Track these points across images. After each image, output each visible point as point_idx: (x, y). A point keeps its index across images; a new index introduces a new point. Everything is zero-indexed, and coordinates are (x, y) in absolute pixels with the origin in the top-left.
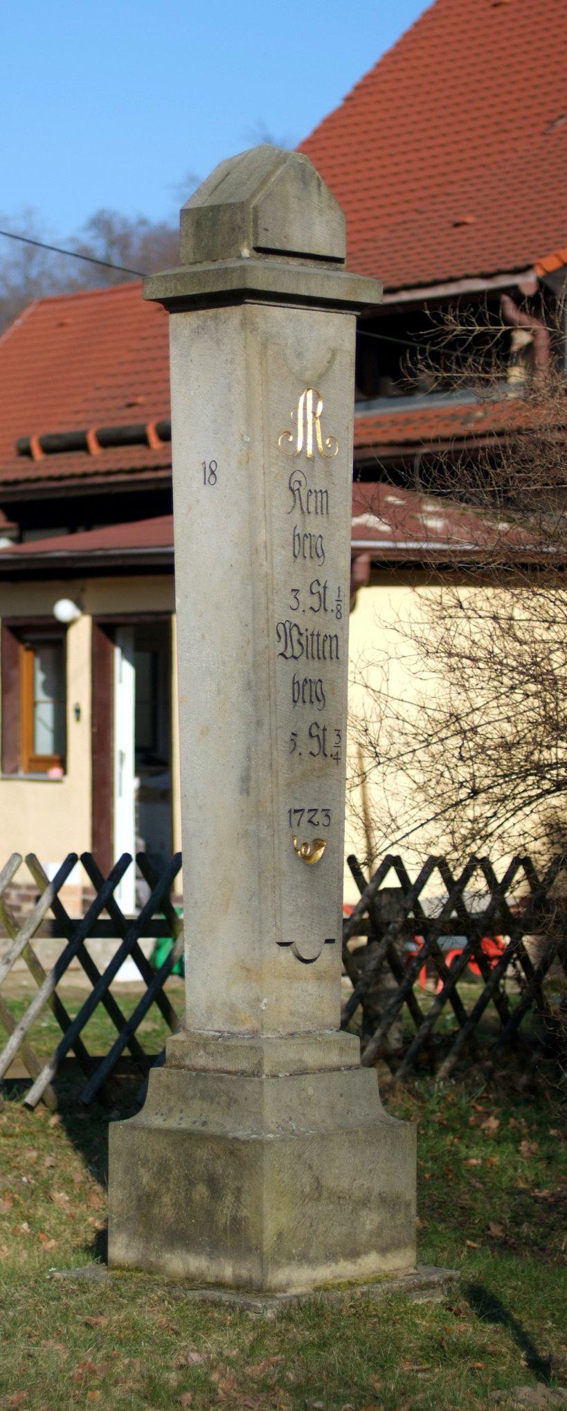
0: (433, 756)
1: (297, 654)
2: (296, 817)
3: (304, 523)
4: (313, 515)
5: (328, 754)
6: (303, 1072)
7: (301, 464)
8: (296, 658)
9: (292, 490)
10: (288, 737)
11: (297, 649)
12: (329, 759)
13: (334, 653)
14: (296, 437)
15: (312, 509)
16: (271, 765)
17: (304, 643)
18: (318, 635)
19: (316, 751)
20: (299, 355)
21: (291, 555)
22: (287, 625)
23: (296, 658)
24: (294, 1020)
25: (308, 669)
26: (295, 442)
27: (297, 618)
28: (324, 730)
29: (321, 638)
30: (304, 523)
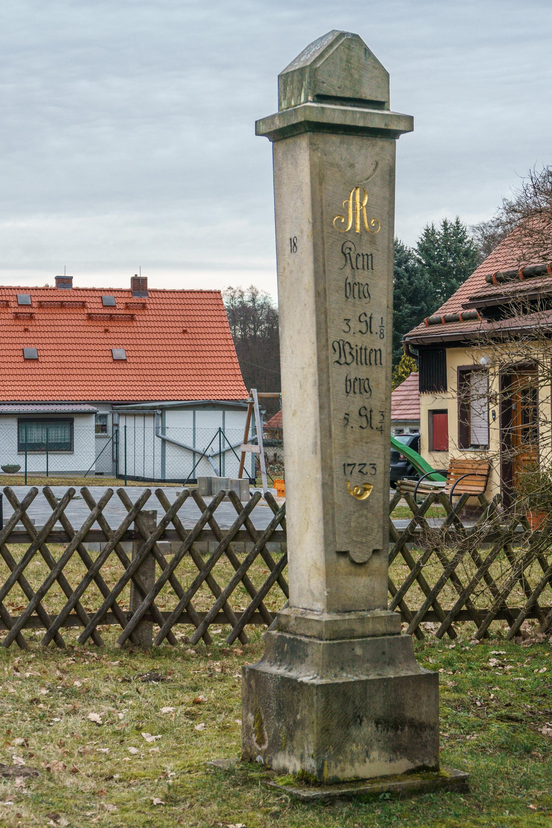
7: (350, 237)
10: (342, 416)
11: (349, 359)
13: (370, 265)
15: (360, 266)
17: (354, 354)
18: (366, 349)
19: (364, 425)
22: (341, 343)
27: (348, 338)
29: (368, 352)
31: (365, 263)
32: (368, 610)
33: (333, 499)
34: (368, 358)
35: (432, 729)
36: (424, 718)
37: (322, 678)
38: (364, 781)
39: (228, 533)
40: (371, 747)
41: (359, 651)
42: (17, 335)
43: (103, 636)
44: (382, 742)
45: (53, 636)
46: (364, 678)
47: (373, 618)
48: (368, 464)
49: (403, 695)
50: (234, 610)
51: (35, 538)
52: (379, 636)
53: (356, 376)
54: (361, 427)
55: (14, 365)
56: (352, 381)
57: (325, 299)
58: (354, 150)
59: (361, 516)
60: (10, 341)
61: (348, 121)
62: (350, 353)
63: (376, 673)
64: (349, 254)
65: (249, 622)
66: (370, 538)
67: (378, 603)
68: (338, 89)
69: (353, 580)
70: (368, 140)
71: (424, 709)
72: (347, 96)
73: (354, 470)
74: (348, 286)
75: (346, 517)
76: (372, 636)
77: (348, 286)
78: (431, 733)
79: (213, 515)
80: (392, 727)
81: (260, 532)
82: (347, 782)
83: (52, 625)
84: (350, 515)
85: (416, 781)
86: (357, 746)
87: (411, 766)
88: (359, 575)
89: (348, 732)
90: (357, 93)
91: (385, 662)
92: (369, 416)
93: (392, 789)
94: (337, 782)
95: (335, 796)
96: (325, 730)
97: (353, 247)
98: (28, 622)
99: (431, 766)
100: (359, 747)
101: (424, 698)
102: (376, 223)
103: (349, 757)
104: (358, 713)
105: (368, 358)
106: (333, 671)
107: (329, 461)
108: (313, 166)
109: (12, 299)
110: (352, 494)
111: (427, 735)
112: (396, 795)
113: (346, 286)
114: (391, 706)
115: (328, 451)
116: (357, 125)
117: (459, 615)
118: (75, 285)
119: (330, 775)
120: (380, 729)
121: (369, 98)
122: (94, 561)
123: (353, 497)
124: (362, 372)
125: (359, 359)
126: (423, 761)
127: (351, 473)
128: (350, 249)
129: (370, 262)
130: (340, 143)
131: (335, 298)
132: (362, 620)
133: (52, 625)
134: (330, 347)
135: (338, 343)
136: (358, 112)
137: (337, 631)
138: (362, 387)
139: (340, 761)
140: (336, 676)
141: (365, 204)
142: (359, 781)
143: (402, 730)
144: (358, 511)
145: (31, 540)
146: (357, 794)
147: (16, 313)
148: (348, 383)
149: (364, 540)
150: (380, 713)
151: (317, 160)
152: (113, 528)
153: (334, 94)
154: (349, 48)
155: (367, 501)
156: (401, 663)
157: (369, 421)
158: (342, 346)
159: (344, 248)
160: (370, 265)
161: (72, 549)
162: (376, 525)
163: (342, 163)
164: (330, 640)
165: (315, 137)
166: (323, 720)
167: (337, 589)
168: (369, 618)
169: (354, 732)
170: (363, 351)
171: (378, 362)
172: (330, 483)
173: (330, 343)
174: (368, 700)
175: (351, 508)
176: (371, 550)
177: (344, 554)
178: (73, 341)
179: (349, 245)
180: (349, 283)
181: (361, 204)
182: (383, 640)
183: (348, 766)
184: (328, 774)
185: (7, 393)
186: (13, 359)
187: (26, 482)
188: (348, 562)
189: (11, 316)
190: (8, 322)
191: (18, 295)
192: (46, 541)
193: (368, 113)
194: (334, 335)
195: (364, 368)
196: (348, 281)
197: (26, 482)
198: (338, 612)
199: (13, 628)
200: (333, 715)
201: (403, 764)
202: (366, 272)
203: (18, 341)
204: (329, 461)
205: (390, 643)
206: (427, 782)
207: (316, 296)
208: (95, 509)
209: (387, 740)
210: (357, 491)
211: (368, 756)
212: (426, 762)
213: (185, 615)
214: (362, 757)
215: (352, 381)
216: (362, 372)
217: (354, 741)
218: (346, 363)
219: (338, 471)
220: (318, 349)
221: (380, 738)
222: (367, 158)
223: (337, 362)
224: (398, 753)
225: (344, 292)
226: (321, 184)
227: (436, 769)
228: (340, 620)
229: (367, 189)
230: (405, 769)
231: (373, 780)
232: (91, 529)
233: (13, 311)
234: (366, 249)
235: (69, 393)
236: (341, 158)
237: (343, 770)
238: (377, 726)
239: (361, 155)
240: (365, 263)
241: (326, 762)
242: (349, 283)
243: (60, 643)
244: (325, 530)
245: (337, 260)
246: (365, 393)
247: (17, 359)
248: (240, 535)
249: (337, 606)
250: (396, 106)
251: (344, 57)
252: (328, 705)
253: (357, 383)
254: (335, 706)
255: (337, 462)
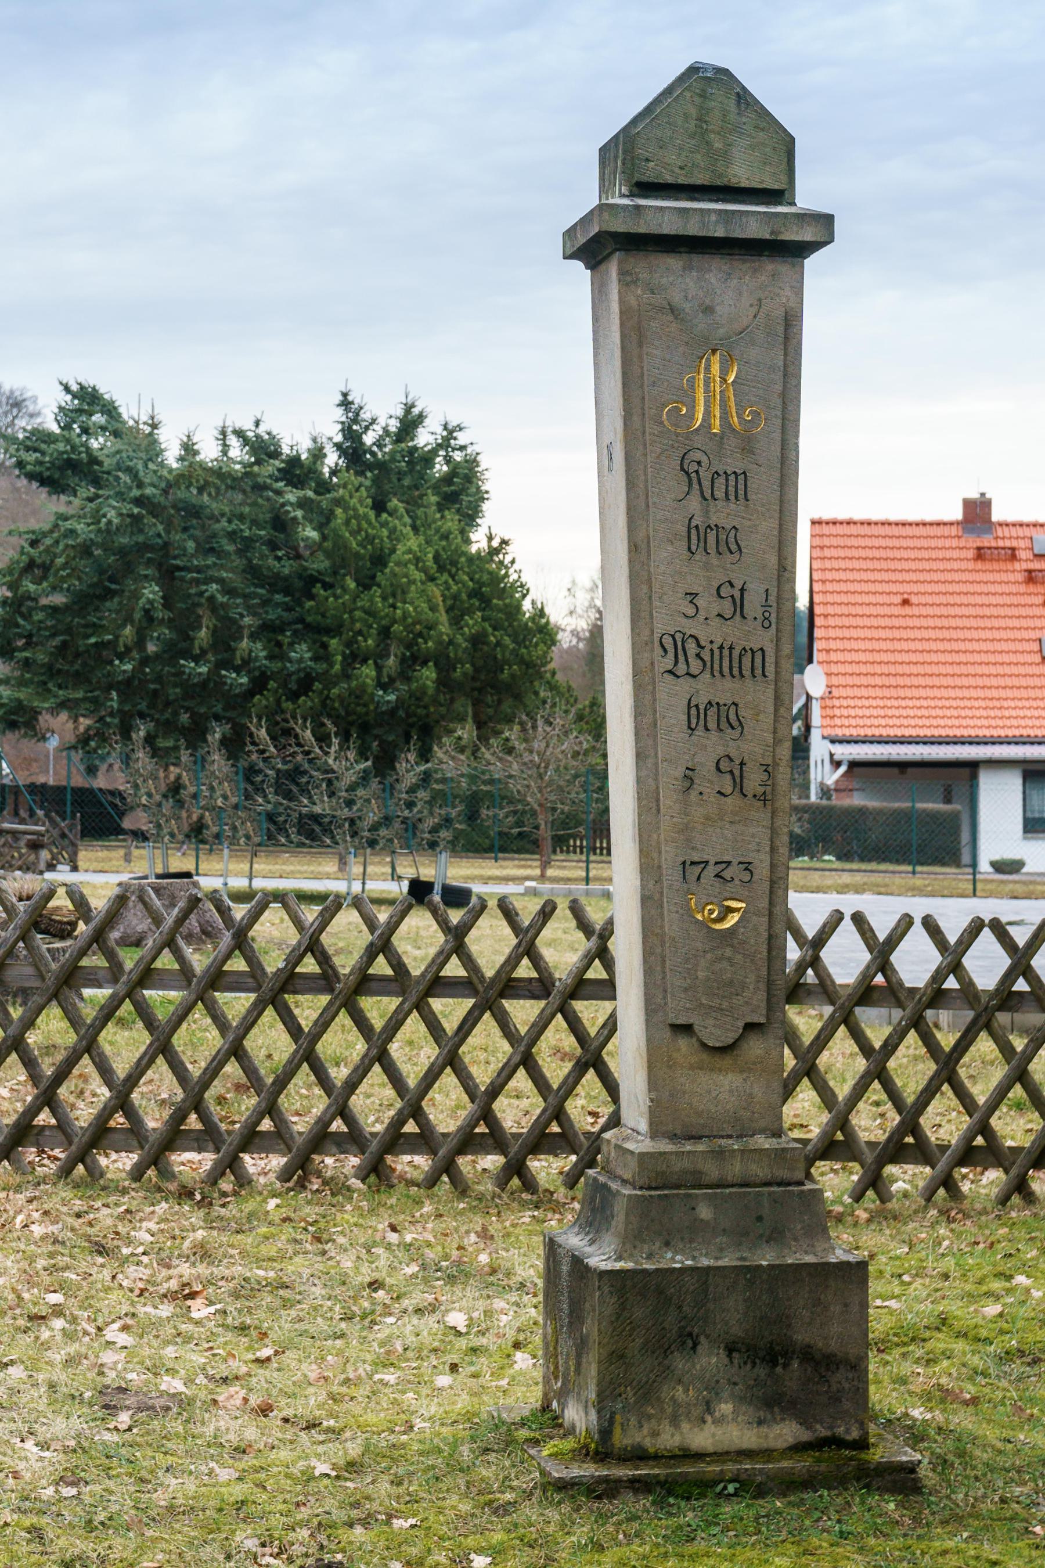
1: (694, 670)
3: (706, 512)
7: (698, 441)
10: (680, 772)
11: (695, 666)
13: (741, 492)
15: (720, 494)
17: (707, 658)
18: (731, 648)
19: (728, 790)
22: (679, 637)
27: (691, 628)
29: (736, 653)
30: (706, 512)
31: (732, 489)
32: (740, 1136)
33: (662, 927)
34: (736, 665)
35: (854, 1367)
36: (834, 1346)
37: (619, 1258)
38: (699, 1456)
39: (850, 991)
40: (717, 1394)
41: (705, 1212)
42: (1029, 611)
43: (966, 1187)
44: (740, 1386)
45: (516, 1168)
46: (705, 1262)
47: (742, 1152)
48: (735, 862)
49: (789, 1299)
50: (864, 1136)
51: (481, 988)
52: (756, 1185)
53: (711, 698)
54: (719, 792)
55: (1022, 670)
56: (702, 707)
57: (649, 555)
58: (713, 280)
59: (720, 959)
60: (1016, 623)
61: (693, 229)
62: (698, 655)
63: (738, 1255)
64: (697, 472)
65: (894, 1160)
66: (738, 1001)
67: (762, 1124)
68: (677, 170)
69: (704, 1079)
70: (744, 262)
71: (835, 1329)
72: (699, 182)
73: (705, 872)
74: (693, 531)
75: (687, 961)
76: (742, 1186)
77: (693, 531)
78: (850, 1376)
79: (821, 954)
80: (763, 1360)
81: (913, 991)
82: (663, 1456)
83: (513, 1150)
84: (695, 956)
85: (802, 1464)
86: (686, 1391)
87: (806, 1436)
88: (720, 1070)
89: (666, 1362)
90: (720, 176)
91: (761, 1236)
92: (737, 773)
93: (743, 1477)
94: (639, 1456)
95: (619, 1481)
96: (616, 1357)
97: (704, 460)
98: (967, 1155)
99: (849, 1438)
100: (691, 1393)
101: (836, 1309)
102: (756, 414)
103: (670, 1410)
104: (688, 1329)
105: (736, 665)
106: (646, 1246)
107: (655, 855)
108: (625, 313)
109: (1022, 544)
110: (699, 917)
111: (840, 1378)
112: (753, 1488)
113: (689, 532)
114: (761, 1318)
115: (655, 836)
116: (710, 234)
117: (540, 1142)
118: (996, 517)
119: (627, 1441)
120: (736, 1361)
121: (744, 184)
122: (593, 1035)
123: (702, 924)
124: (725, 690)
125: (716, 667)
126: (831, 1428)
127: (699, 879)
128: (699, 463)
129: (741, 486)
130: (684, 269)
131: (667, 556)
132: (720, 1154)
133: (513, 1150)
134: (657, 644)
135: (673, 636)
136: (715, 211)
137: (663, 1173)
138: (723, 719)
139: (650, 1417)
140: (650, 1256)
141: (731, 379)
142: (688, 1455)
143: (785, 1366)
144: (713, 949)
145: (475, 993)
146: (666, 1481)
147: (1030, 571)
148: (693, 711)
149: (725, 1005)
150: (737, 1330)
151: (633, 302)
152: (839, 980)
153: (670, 179)
154: (703, 95)
155: (732, 931)
156: (796, 1240)
157: (739, 785)
158: (679, 644)
159: (686, 462)
160: (741, 492)
161: (548, 1011)
162: (751, 979)
163: (687, 306)
164: (650, 1188)
165: (632, 260)
166: (612, 1337)
167: (672, 1095)
168: (734, 1151)
169: (679, 1362)
170: (726, 652)
171: (758, 671)
172: (657, 897)
173: (657, 636)
174: (711, 1306)
175: (699, 945)
176: (741, 1024)
177: (687, 1029)
178: (938, 622)
179: (698, 456)
180: (697, 527)
181: (724, 380)
182: (759, 1194)
183: (666, 1428)
184: (620, 1440)
185: (1008, 723)
186: (1021, 658)
187: (975, 890)
188: (696, 1045)
189: (1020, 577)
190: (1014, 589)
191: (1035, 536)
192: (502, 995)
193: (734, 212)
194: (663, 623)
195: (728, 683)
196: (694, 523)
197: (975, 890)
198: (673, 1137)
199: (440, 1153)
200: (633, 1329)
201: (786, 1432)
202: (732, 506)
203: (1030, 623)
204: (655, 855)
205: (774, 1200)
206: (823, 1467)
207: (630, 552)
208: (594, 938)
209: (752, 1382)
210: (711, 912)
211: (709, 1409)
212: (840, 1430)
213: (837, 1145)
214: (696, 1412)
215: (702, 707)
216: (725, 690)
217: (680, 1382)
218: (688, 674)
219: (671, 875)
220: (633, 649)
221: (736, 1379)
222: (740, 294)
223: (670, 672)
224: (776, 1409)
225: (685, 544)
226: (640, 345)
227: (862, 1444)
228: (671, 1153)
229: (736, 353)
230: (791, 1440)
231: (720, 1456)
232: (442, 974)
233: (1025, 566)
234: (733, 463)
235: (861, 722)
236: (686, 297)
237: (655, 1434)
238: (729, 1356)
239: (728, 291)
240: (732, 489)
241: (618, 1417)
242: (697, 527)
243: (529, 1184)
244: (646, 984)
245: (673, 483)
246: (730, 730)
247: (1029, 658)
248: (875, 995)
249: (670, 1127)
250: (809, 194)
251: (693, 112)
252: (624, 1309)
253: (712, 712)
254: (638, 1313)
255: (669, 857)
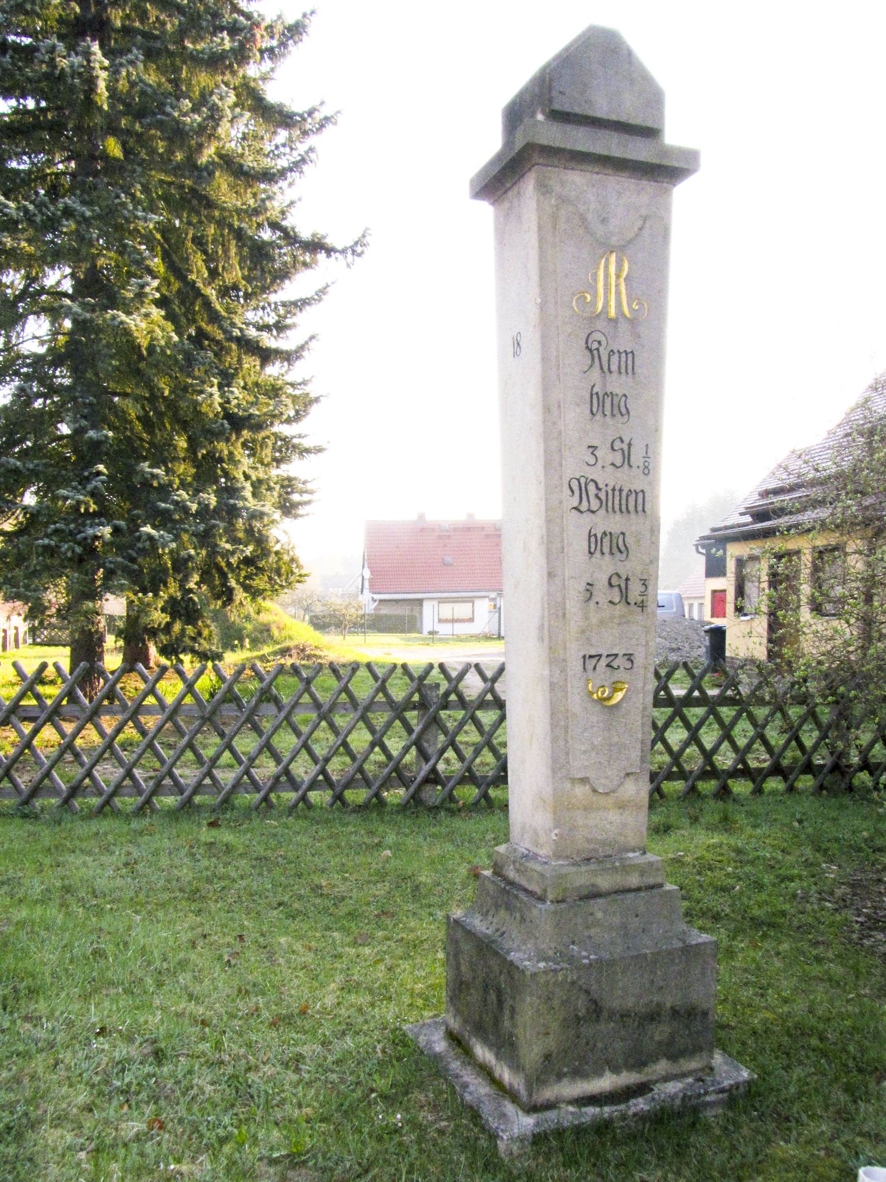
0: (64, 905)
1: (594, 507)
2: (591, 663)
4: (615, 375)
5: (631, 600)
6: (595, 894)
8: (593, 512)
9: (591, 350)
10: (582, 586)
11: (595, 504)
12: (633, 607)
13: (640, 508)
14: (595, 295)
15: (614, 367)
16: (564, 615)
17: (603, 497)
18: (621, 490)
19: (617, 600)
20: (604, 221)
21: (588, 412)
22: (583, 481)
23: (593, 512)
24: (591, 846)
25: (614, 523)
26: (594, 303)
27: (594, 474)
28: (627, 579)
